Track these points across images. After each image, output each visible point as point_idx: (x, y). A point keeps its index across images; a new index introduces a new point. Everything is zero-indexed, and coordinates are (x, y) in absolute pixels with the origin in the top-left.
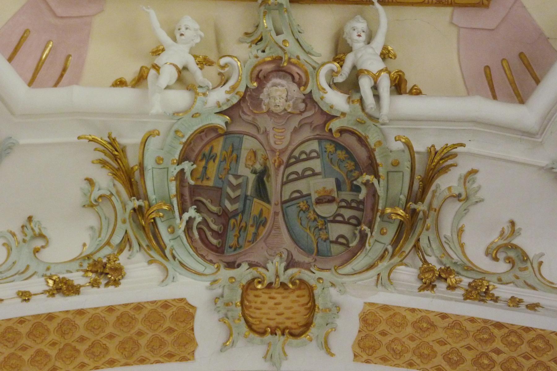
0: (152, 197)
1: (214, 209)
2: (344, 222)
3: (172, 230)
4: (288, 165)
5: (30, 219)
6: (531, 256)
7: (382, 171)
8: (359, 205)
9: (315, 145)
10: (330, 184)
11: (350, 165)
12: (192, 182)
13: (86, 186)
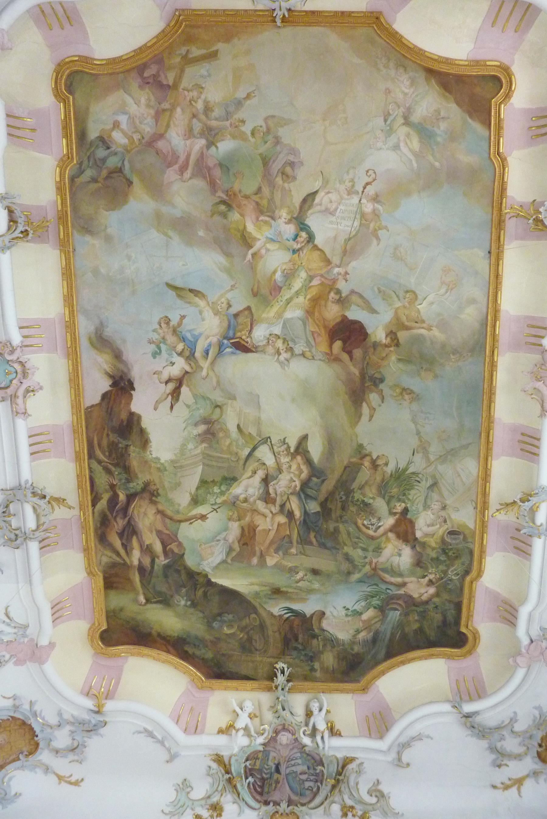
0: (234, 774)
1: (259, 776)
2: (311, 781)
3: (242, 785)
4: (288, 761)
5: (185, 780)
6: (385, 794)
7: (325, 765)
8: (317, 775)
9: (299, 755)
10: (305, 768)
11: (313, 761)
12: (250, 767)
13: (208, 768)
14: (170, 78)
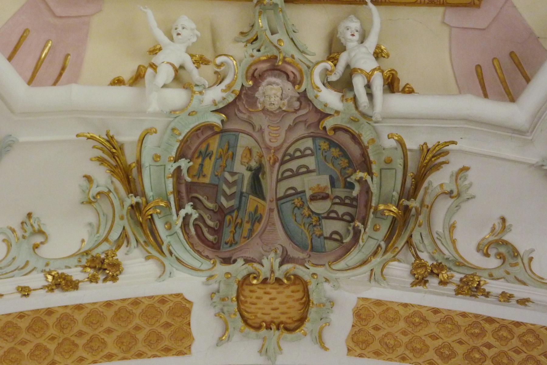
0: (150, 193)
1: (210, 205)
2: (338, 219)
3: (169, 226)
4: (283, 163)
5: (29, 215)
6: (522, 252)
7: (375, 168)
8: (353, 202)
9: (309, 143)
10: (324, 181)
11: (344, 162)
12: (189, 179)
13: (84, 183)
14: (30, 331)
